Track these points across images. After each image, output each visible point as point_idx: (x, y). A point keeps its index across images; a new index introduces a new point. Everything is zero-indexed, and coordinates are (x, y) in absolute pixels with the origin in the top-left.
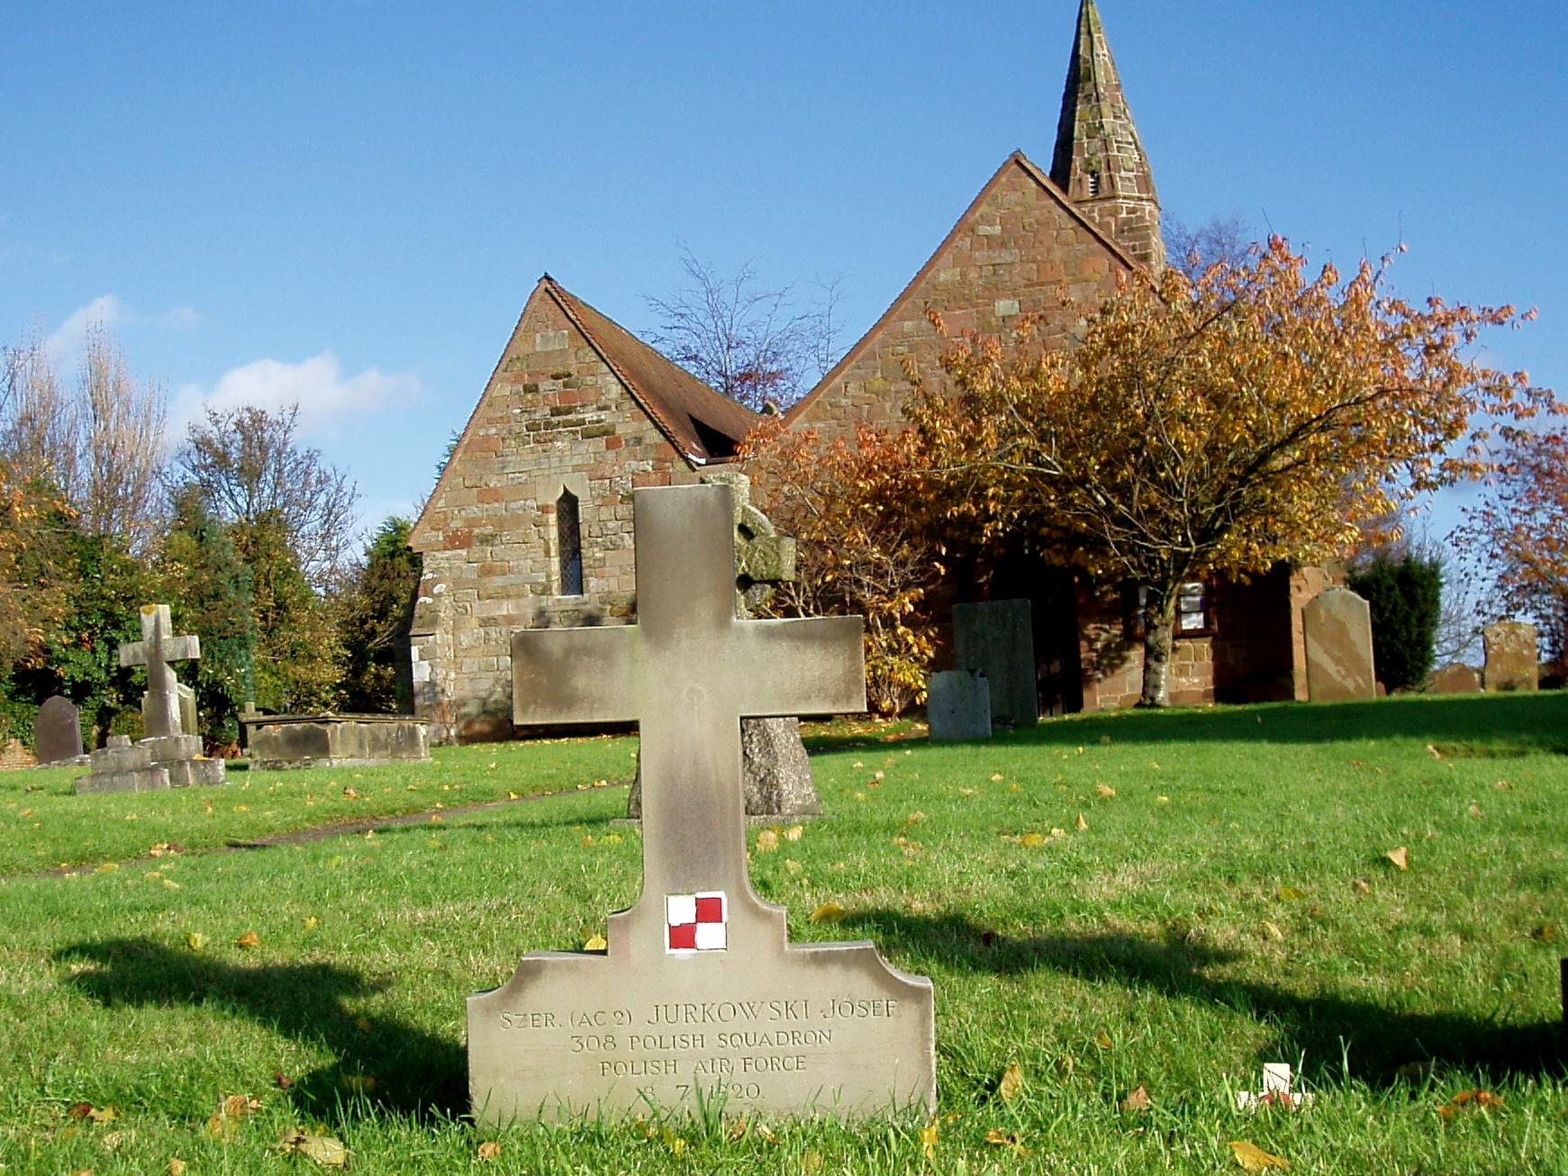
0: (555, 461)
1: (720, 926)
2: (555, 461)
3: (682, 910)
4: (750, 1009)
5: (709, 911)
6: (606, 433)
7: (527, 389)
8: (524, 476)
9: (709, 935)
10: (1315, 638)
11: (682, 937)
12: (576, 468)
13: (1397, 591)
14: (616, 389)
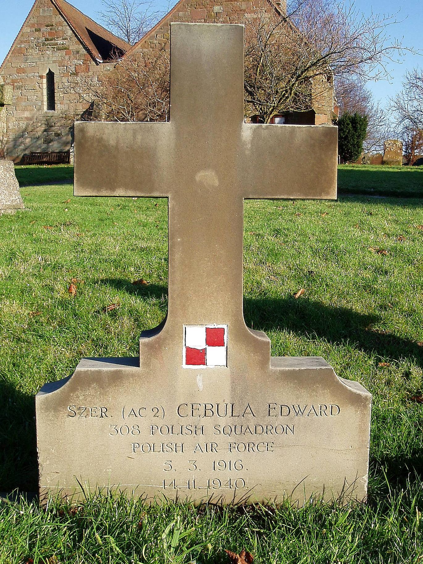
2: (46, 58)
3: (196, 337)
5: (214, 338)
6: (65, 49)
9: (216, 356)
11: (196, 357)
12: (54, 62)
14: (70, 32)
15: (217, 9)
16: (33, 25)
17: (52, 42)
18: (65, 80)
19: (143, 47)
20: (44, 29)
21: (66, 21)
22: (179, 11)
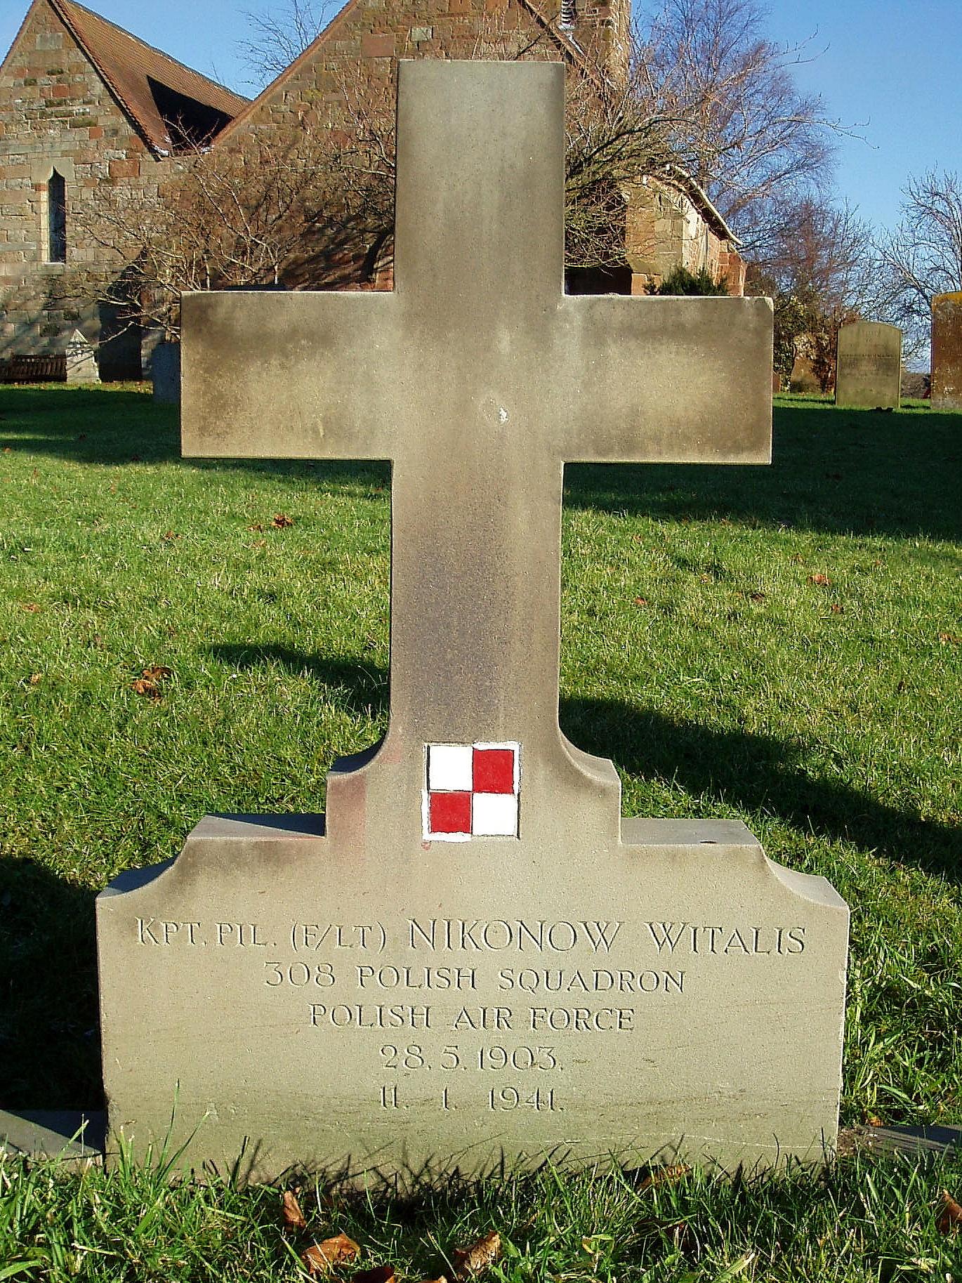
0: (47, 145)
2: (47, 145)
3: (451, 768)
4: (544, 937)
5: (493, 773)
6: (89, 124)
7: (27, 83)
8: (23, 158)
9: (493, 813)
11: (452, 812)
12: (65, 154)
14: (99, 87)
15: (418, 32)
16: (20, 72)
17: (61, 108)
18: (87, 194)
19: (257, 120)
20: (43, 80)
21: (90, 61)
22: (335, 38)
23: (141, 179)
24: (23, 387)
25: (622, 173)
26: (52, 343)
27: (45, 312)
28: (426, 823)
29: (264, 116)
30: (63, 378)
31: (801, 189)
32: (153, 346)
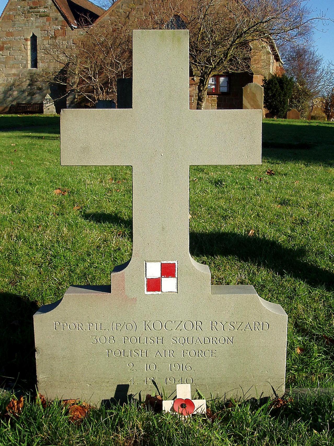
1: (175, 279)
5: (168, 270)
6: (46, 16)
8: (21, 29)
9: (168, 284)
10: (245, 97)
11: (154, 285)
12: (37, 27)
13: (278, 85)
19: (111, 15)
23: (66, 37)
24: (27, 115)
25: (250, 38)
26: (32, 99)
27: (29, 87)
28: (146, 289)
29: (113, 14)
30: (41, 111)
31: (300, 42)
32: (71, 100)
